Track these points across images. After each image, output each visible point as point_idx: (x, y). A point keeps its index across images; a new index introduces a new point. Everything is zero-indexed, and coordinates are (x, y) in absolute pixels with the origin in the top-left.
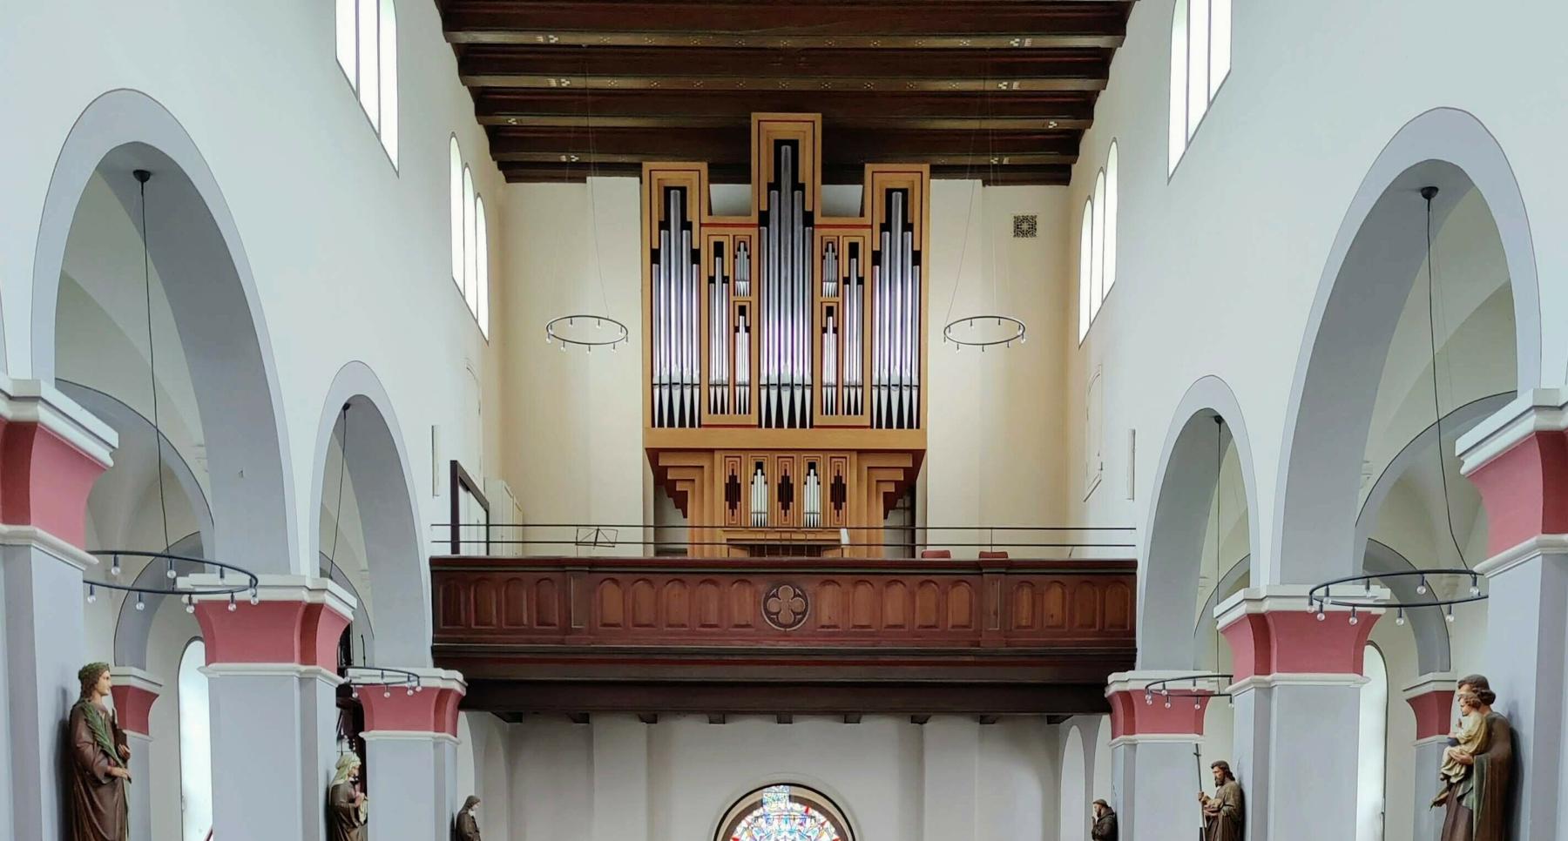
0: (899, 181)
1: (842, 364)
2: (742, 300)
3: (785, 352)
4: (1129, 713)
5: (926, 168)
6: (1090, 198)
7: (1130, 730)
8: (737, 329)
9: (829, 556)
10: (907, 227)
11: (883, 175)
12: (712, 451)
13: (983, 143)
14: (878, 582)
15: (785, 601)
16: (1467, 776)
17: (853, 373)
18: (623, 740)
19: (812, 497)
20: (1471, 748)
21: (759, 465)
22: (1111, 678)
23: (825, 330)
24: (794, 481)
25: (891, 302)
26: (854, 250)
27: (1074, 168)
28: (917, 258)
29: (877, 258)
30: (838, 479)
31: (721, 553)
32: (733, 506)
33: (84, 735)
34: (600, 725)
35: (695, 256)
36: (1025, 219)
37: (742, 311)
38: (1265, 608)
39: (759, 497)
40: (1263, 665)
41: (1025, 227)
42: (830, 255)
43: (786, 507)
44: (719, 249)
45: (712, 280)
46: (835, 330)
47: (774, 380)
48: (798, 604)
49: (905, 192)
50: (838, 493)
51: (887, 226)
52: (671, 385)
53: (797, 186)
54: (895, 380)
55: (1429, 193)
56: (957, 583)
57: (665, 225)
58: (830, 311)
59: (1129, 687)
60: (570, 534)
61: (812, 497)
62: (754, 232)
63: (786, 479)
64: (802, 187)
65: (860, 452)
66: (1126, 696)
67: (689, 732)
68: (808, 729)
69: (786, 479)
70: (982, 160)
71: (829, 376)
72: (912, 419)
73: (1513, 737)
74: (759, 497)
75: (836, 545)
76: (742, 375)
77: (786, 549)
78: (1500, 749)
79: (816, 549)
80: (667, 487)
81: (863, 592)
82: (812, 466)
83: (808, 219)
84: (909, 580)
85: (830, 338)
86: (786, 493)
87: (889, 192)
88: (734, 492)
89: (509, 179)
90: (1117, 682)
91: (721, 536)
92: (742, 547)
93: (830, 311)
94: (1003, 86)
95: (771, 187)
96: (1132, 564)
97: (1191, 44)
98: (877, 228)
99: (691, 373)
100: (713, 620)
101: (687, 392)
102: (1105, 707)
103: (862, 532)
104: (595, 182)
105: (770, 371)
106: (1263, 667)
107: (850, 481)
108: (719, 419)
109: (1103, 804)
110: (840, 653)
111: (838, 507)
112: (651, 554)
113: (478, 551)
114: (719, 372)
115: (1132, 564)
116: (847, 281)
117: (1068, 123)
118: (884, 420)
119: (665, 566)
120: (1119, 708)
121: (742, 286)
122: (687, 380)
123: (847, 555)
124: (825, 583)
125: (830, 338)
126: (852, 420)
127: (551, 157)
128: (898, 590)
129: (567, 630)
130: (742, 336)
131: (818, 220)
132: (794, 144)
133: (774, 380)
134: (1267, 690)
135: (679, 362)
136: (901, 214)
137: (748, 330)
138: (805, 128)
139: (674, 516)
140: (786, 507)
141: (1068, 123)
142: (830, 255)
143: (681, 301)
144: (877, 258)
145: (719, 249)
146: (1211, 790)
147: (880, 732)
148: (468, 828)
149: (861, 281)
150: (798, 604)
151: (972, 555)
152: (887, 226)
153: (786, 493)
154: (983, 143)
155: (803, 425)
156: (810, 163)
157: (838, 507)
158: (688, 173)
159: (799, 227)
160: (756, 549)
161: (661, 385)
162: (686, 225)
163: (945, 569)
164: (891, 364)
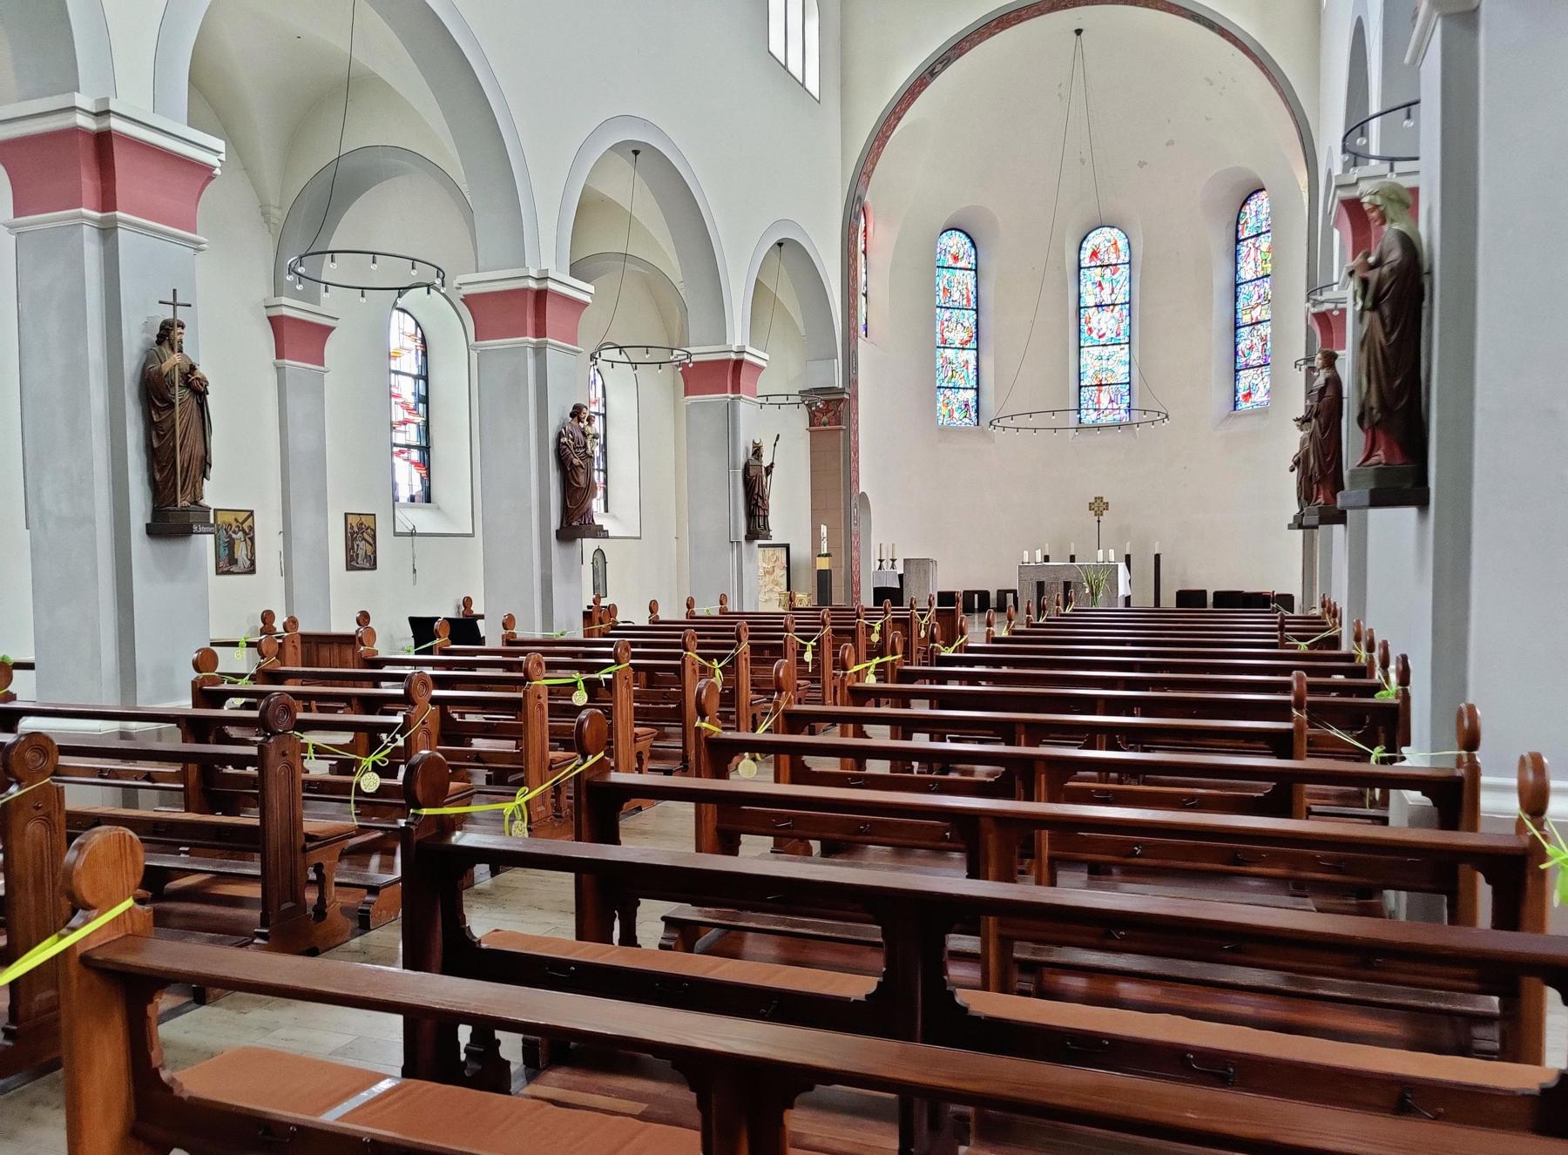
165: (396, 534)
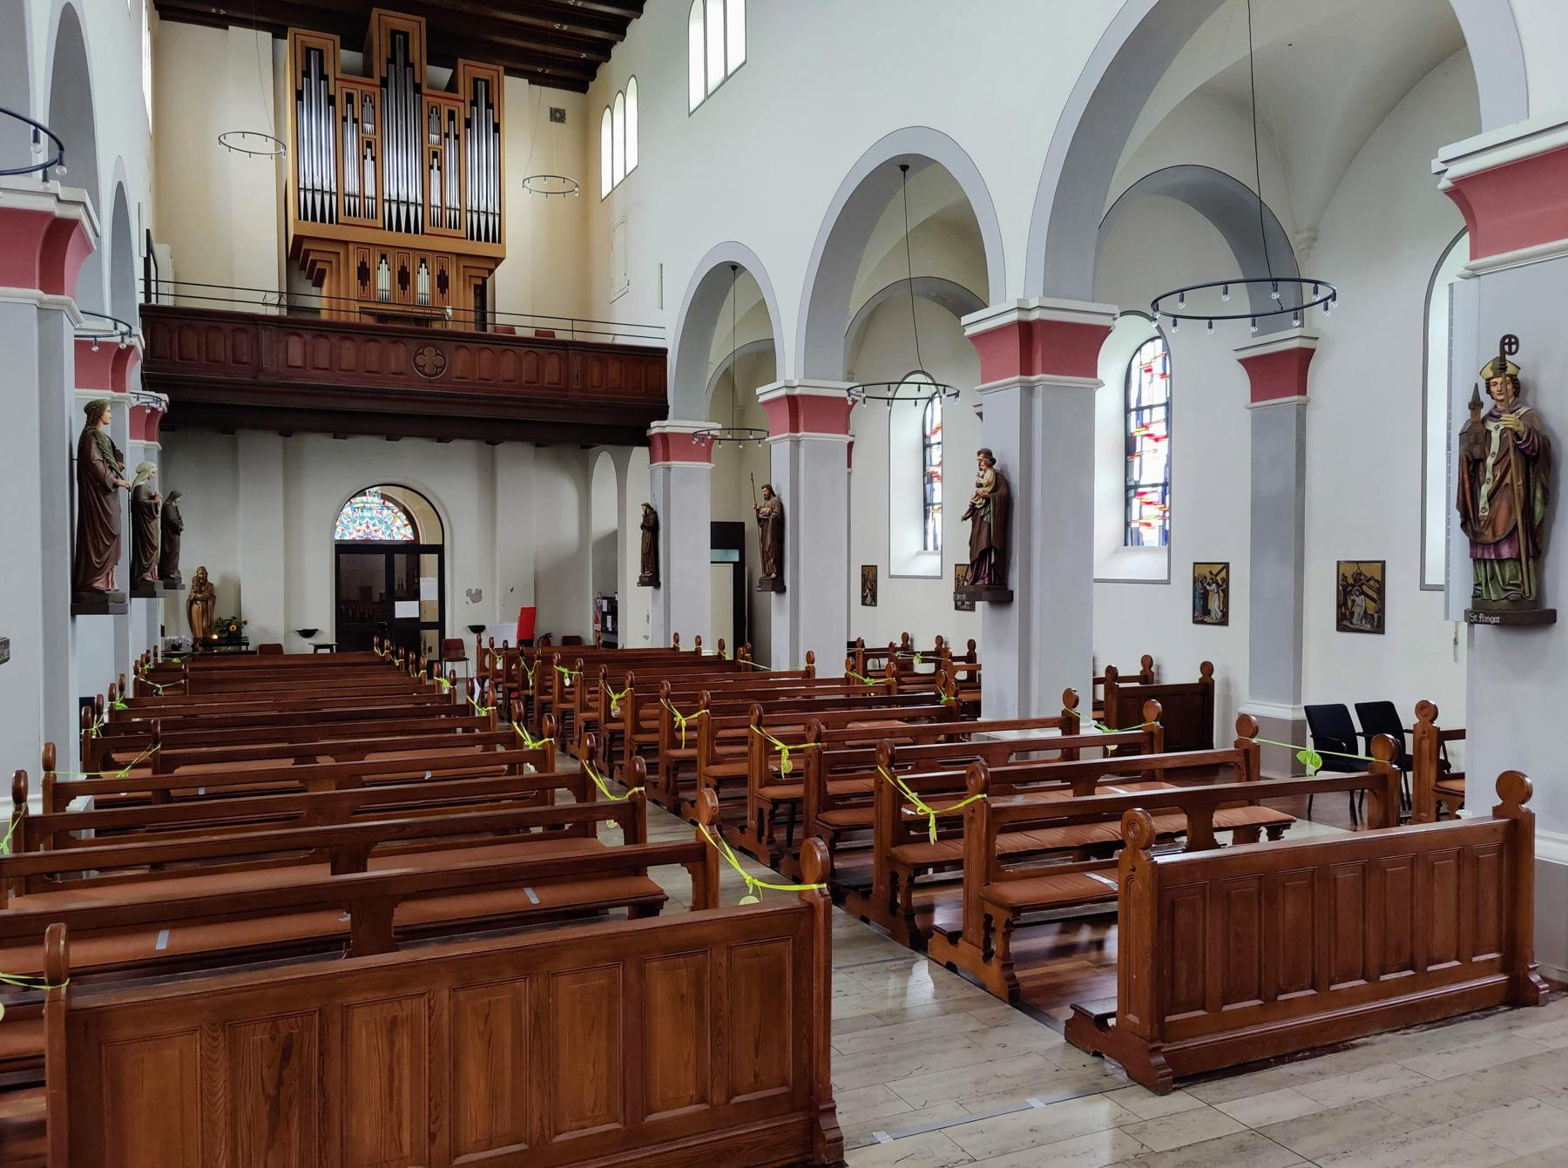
0: (483, 74)
1: (443, 193)
2: (370, 137)
3: (401, 178)
4: (664, 448)
5: (501, 69)
6: (611, 107)
7: (668, 459)
8: (365, 157)
9: (437, 326)
10: (489, 106)
11: (469, 69)
12: (346, 243)
13: (546, 59)
14: (334, 339)
15: (429, 358)
16: (986, 505)
17: (452, 200)
18: (264, 448)
19: (423, 282)
20: (989, 489)
21: (423, 261)
22: (653, 424)
23: (431, 167)
24: (370, 265)
25: (477, 151)
26: (451, 115)
27: (591, 84)
28: (497, 128)
29: (468, 124)
30: (443, 272)
31: (354, 318)
32: (363, 284)
33: (96, 455)
34: (246, 439)
35: (331, 101)
36: (557, 110)
37: (369, 145)
38: (797, 391)
39: (384, 279)
40: (794, 428)
41: (557, 116)
42: (434, 116)
43: (404, 288)
44: (350, 98)
45: (345, 119)
46: (439, 168)
47: (394, 197)
48: (439, 360)
49: (487, 82)
50: (442, 282)
51: (474, 103)
52: (313, 191)
53: (409, 64)
54: (483, 208)
55: (904, 168)
56: (459, 347)
57: (306, 74)
58: (435, 155)
59: (667, 430)
60: (259, 297)
61: (423, 282)
62: (377, 91)
63: (403, 268)
64: (412, 65)
65: (458, 255)
66: (664, 436)
67: (317, 444)
68: (409, 447)
69: (403, 268)
70: (532, 68)
71: (436, 200)
72: (496, 237)
73: (1007, 484)
74: (384, 279)
75: (442, 318)
76: (370, 190)
77: (406, 319)
78: (1002, 490)
79: (426, 321)
80: (301, 259)
81: (373, 347)
82: (423, 261)
83: (417, 88)
84: (517, 350)
85: (435, 173)
86: (404, 278)
87: (476, 80)
88: (364, 274)
89: (162, 18)
90: (656, 427)
91: (356, 306)
92: (369, 314)
93: (435, 155)
94: (557, 26)
95: (389, 61)
96: (665, 351)
97: (710, 23)
98: (468, 102)
99: (329, 183)
100: (374, 367)
101: (327, 198)
102: (646, 441)
103: (456, 311)
104: (233, 30)
105: (391, 190)
106: (794, 428)
107: (452, 275)
108: (352, 220)
109: (648, 506)
110: (442, 395)
111: (443, 292)
112: (284, 312)
113: (167, 301)
114: (352, 185)
115: (665, 351)
116: (447, 135)
117: (593, 57)
118: (475, 235)
119: (295, 322)
120: (658, 444)
121: (369, 127)
122: (326, 188)
123: (450, 326)
124: (343, 338)
125: (435, 173)
126: (453, 232)
127: (203, 8)
128: (463, 352)
129: (260, 369)
130: (369, 163)
131: (425, 90)
132: (406, 35)
133: (394, 197)
134: (796, 443)
135: (319, 172)
136: (486, 98)
137: (373, 159)
138: (415, 26)
139: (306, 287)
140: (404, 288)
141: (593, 57)
142: (434, 116)
143: (318, 129)
144: (468, 124)
145: (350, 98)
146: (761, 502)
147: (464, 451)
148: (173, 516)
149: (457, 137)
150: (439, 360)
151: (530, 333)
152: (474, 103)
153: (404, 278)
154: (546, 59)
155: (416, 231)
156: (417, 49)
157: (443, 292)
158: (326, 41)
159: (410, 93)
160: (382, 317)
161: (305, 190)
162: (323, 77)
163: (507, 340)
164: (480, 196)
165: (1424, 587)
